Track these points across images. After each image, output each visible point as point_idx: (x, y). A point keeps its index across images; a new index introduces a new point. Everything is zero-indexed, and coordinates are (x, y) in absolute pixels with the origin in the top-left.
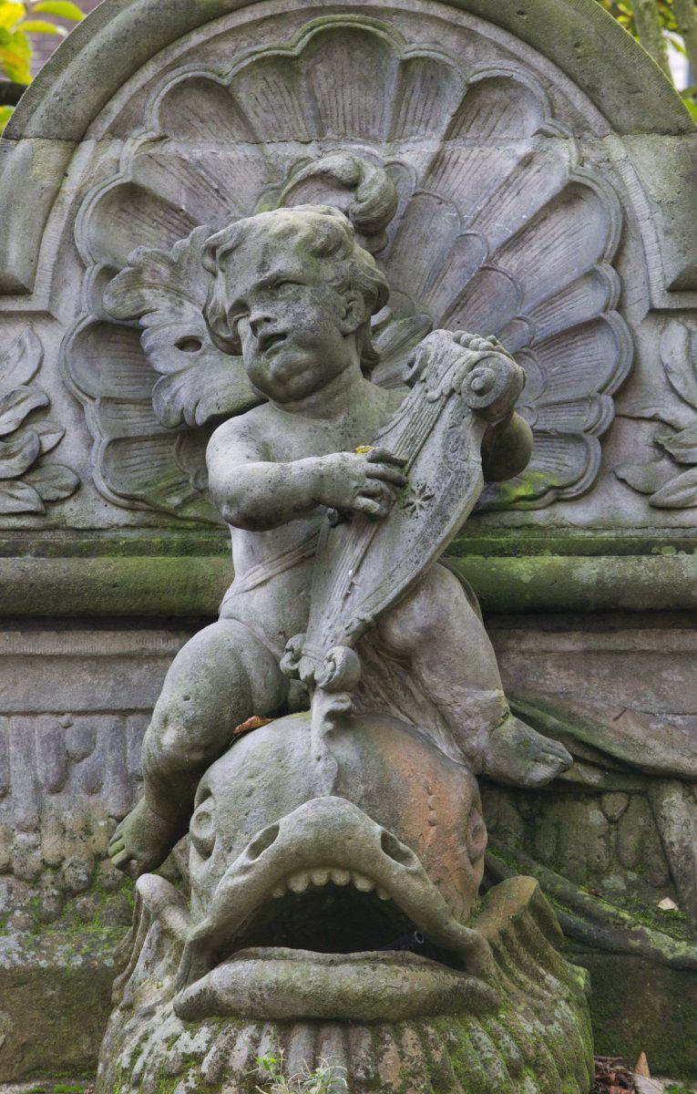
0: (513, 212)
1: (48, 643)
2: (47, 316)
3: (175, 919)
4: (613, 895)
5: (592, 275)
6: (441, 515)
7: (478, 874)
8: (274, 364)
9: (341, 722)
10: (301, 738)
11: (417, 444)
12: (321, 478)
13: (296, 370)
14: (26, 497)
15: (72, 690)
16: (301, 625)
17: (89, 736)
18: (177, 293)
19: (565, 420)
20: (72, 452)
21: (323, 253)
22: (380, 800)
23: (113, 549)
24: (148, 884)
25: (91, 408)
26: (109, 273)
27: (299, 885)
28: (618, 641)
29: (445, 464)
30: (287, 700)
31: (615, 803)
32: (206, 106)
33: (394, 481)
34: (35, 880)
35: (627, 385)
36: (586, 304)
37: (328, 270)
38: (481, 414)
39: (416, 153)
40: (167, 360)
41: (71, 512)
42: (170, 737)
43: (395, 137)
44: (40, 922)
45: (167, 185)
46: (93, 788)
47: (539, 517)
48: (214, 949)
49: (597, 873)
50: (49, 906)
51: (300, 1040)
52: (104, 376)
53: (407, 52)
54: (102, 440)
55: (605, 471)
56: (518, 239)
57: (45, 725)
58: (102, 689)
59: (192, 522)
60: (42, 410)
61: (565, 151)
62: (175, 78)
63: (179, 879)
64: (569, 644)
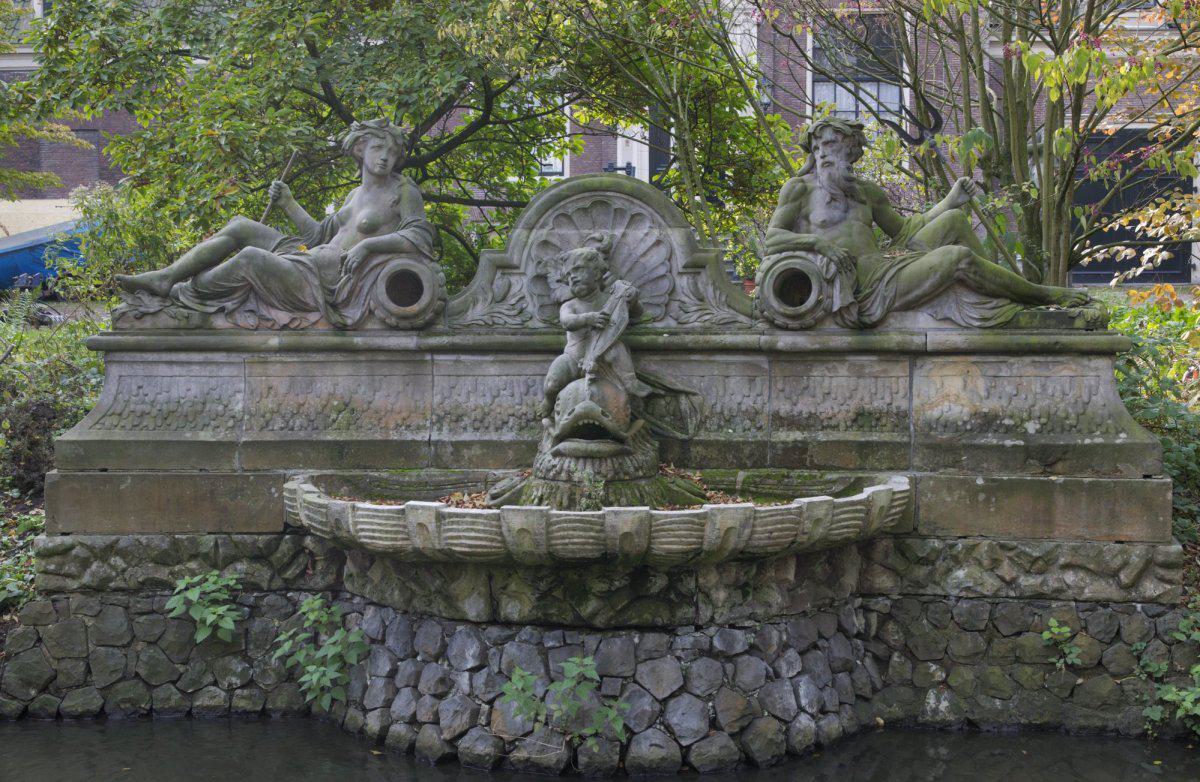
0: (643, 247)
1: (524, 358)
2: (524, 274)
3: (551, 430)
4: (667, 423)
5: (663, 263)
6: (618, 328)
7: (628, 419)
8: (577, 289)
9: (593, 381)
10: (582, 385)
11: (612, 310)
12: (587, 319)
13: (582, 290)
14: (518, 320)
15: (530, 369)
16: (583, 355)
17: (534, 381)
18: (556, 268)
19: (656, 301)
20: (530, 309)
21: (590, 260)
22: (602, 401)
23: (540, 334)
24: (545, 421)
25: (535, 297)
26: (539, 263)
27: (581, 423)
28: (670, 358)
29: (619, 316)
30: (580, 375)
31: (668, 399)
32: (565, 220)
33: (607, 319)
34: (520, 418)
35: (672, 291)
36: (662, 271)
37: (592, 264)
38: (628, 302)
39: (618, 232)
40: (554, 285)
41: (530, 324)
42: (550, 384)
43: (613, 228)
44: (521, 429)
45: (554, 240)
46: (535, 395)
47: (649, 325)
48: (559, 439)
49: (663, 416)
50: (523, 424)
51: (581, 461)
52: (538, 289)
53: (616, 206)
54: (538, 305)
55: (666, 314)
56: (644, 254)
57: (523, 378)
58: (538, 369)
59: (555, 326)
60: (522, 298)
61: (656, 232)
62: (558, 212)
63: (553, 420)
64: (656, 358)
